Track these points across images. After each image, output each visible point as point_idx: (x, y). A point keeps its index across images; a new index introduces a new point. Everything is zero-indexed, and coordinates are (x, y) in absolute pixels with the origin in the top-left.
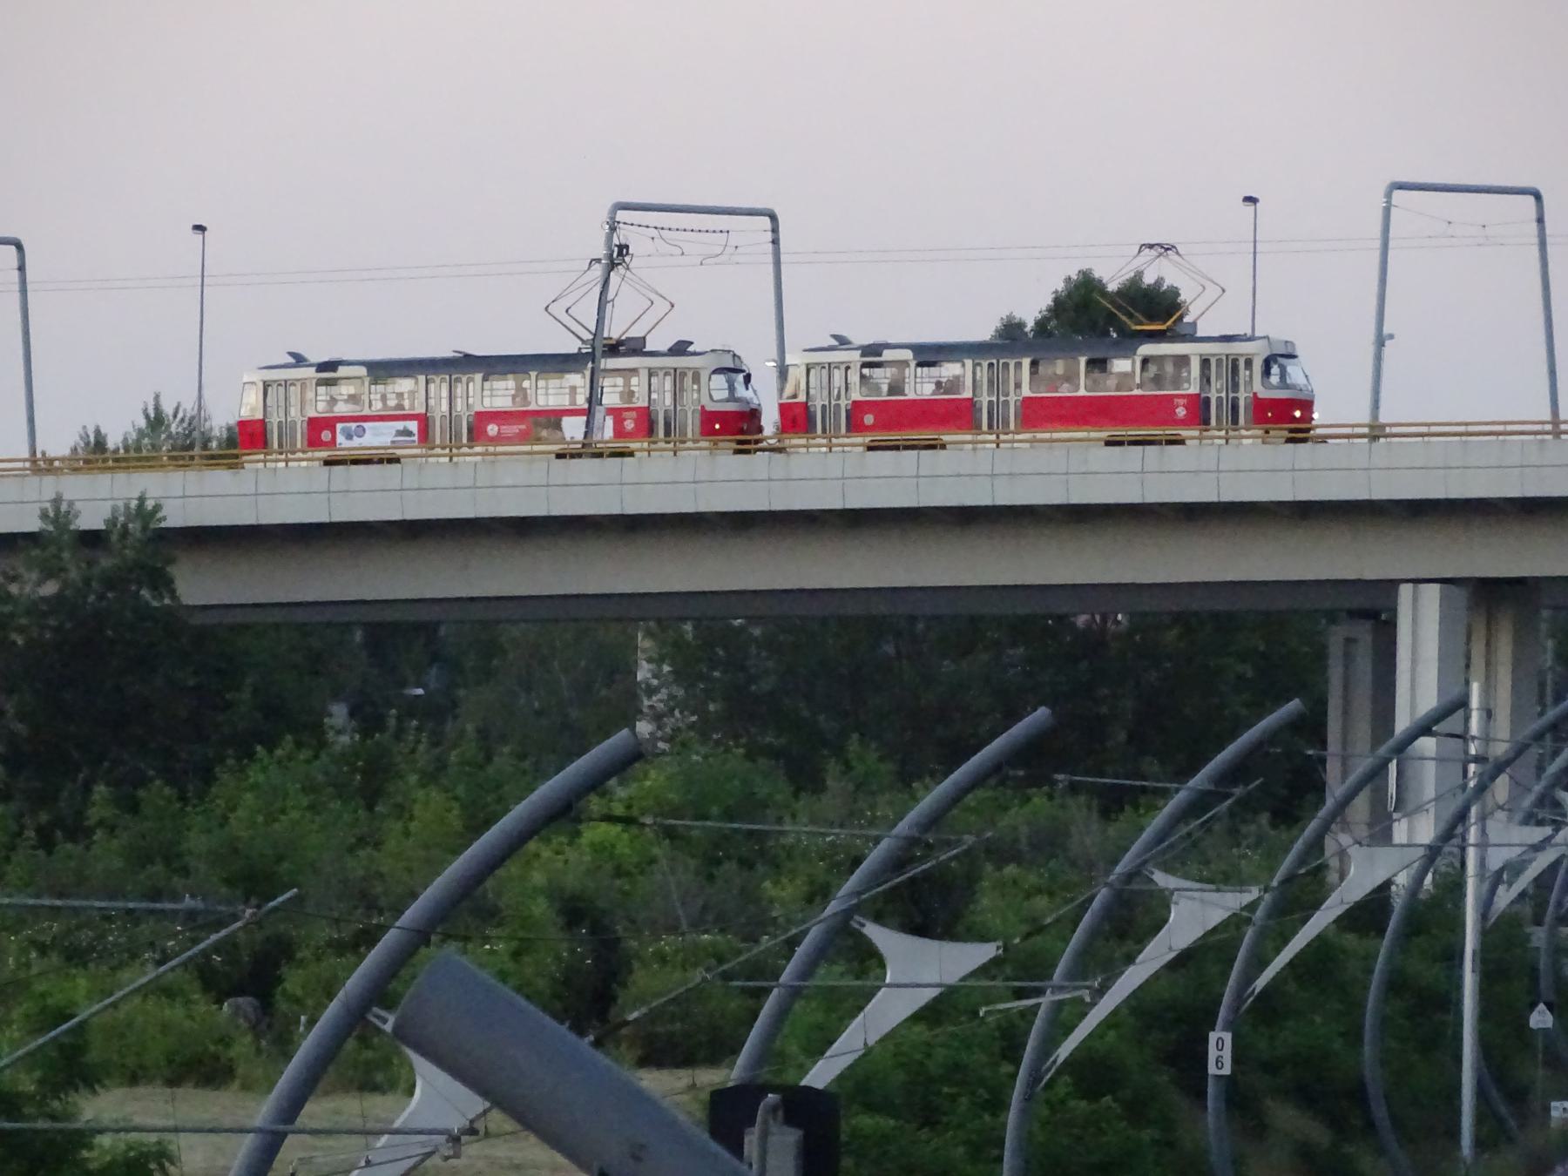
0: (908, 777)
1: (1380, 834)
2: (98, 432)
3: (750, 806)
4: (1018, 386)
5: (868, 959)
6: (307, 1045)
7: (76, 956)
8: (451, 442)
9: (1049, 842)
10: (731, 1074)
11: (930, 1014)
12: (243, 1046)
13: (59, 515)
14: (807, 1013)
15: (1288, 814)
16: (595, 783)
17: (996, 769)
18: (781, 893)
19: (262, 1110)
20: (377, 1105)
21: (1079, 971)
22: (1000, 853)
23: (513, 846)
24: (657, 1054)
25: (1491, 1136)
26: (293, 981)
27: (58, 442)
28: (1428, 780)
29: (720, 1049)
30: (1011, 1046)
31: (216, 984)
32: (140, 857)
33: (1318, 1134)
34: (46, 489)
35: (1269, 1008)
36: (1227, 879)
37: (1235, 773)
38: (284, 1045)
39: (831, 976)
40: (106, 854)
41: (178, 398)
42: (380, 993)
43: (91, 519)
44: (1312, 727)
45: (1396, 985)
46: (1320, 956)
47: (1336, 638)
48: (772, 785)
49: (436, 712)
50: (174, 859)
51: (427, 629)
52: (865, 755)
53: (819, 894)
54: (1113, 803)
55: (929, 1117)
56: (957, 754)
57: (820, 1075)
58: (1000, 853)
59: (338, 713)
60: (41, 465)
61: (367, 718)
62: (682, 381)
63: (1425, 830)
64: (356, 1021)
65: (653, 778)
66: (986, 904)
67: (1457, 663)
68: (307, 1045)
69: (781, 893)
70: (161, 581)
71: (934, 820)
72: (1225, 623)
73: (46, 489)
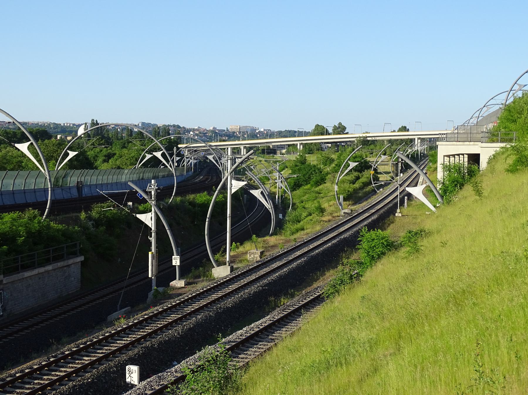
2: (340, 124)
43: (364, 136)
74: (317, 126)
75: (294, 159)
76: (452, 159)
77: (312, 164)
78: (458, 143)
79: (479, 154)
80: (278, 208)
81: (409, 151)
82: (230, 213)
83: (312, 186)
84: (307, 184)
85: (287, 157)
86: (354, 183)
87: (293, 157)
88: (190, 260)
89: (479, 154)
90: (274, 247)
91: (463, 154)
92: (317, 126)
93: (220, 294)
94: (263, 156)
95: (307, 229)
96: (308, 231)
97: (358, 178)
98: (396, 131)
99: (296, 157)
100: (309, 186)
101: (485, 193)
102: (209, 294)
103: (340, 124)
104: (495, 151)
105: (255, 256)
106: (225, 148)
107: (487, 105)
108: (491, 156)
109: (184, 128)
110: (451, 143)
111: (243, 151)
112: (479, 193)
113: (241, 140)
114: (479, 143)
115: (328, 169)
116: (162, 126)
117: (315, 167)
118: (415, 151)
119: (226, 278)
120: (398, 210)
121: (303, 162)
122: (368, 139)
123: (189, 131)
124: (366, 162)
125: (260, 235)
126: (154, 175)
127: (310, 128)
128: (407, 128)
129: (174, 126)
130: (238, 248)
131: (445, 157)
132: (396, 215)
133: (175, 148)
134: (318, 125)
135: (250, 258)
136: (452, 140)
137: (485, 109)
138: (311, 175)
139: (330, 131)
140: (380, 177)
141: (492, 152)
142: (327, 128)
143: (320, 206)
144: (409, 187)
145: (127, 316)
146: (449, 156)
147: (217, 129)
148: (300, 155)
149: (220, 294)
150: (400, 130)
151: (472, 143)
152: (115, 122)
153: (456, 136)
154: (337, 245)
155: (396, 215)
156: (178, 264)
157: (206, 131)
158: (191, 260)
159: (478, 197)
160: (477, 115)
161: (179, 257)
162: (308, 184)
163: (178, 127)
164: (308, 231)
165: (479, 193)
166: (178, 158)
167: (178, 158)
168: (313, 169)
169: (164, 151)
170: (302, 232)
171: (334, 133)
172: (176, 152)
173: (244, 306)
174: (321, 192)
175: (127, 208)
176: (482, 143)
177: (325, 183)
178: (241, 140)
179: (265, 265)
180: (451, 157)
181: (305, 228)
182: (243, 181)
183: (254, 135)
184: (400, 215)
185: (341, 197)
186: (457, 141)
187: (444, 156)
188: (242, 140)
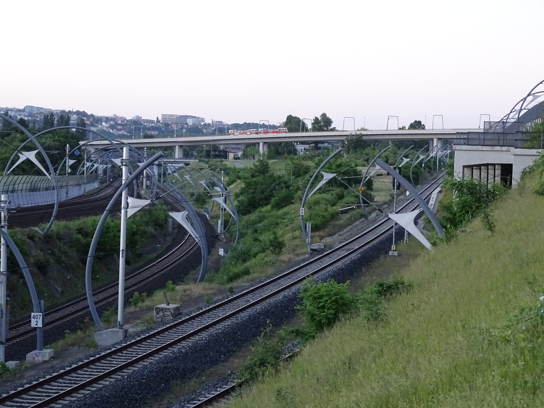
0: (405, 149)
1: (433, 153)
2: (324, 115)
3: (396, 151)
4: (57, 290)
5: (403, 160)
6: (370, 165)
7: (357, 159)
8: (424, 199)
9: (414, 153)
10: (395, 166)
11: (406, 163)
12: (366, 165)
13: (356, 134)
14: (399, 163)
15: (427, 152)
16: (387, 149)
17: (410, 149)
18: (398, 156)
19: (368, 168)
20: (374, 168)
21: (415, 160)
22: (410, 154)
23: (382, 153)
24: (390, 165)
25: (439, 170)
26: (369, 161)
27: (356, 129)
28: (435, 150)
29: (394, 165)
30: (411, 165)
31: (365, 161)
32: (360, 153)
33: (429, 170)
34: (355, 132)
35: (426, 163)
36: (424, 155)
37: (424, 149)
38: (369, 164)
39: (401, 161)
40: (359, 153)
41: (363, 127)
42: (374, 161)
43: (358, 134)
44: (429, 146)
45: (433, 161)
46: (429, 160)
47: (430, 141)
48: (397, 149)
49: (378, 145)
50: (363, 154)
51: (377, 140)
52: (403, 148)
53: (400, 156)
54: (417, 151)
55: (406, 169)
56: (408, 148)
57: (400, 166)
58: (410, 154)
59: (372, 145)
60: (355, 131)
61: (374, 145)
62: (323, 250)
63: (435, 153)
64: (373, 163)
65: (391, 149)
66: (410, 156)
67: (437, 143)
68: (370, 165)
69: (398, 156)
70: (362, 137)
71: (407, 151)
72: (424, 140)
73: (355, 132)
74: (290, 118)
75: (252, 166)
76: (476, 172)
77: (277, 175)
78: (485, 148)
79: (512, 165)
80: (219, 240)
81: (422, 157)
82: (123, 245)
83: (273, 207)
84: (267, 204)
85: (240, 164)
86: (333, 205)
87: (249, 164)
88: (68, 319)
89: (512, 165)
90: (198, 299)
91: (494, 165)
92: (290, 118)
93: (96, 373)
94: (206, 160)
95: (254, 273)
96: (255, 275)
97: (341, 197)
98: (407, 128)
99: (254, 164)
100: (269, 207)
101: (499, 227)
102: (78, 374)
103: (324, 115)
104: (535, 162)
105: (166, 313)
106: (144, 148)
107: (532, 93)
108: (525, 169)
109: (92, 116)
110: (475, 148)
111: (178, 153)
112: (491, 227)
113: (175, 136)
114: (512, 149)
115: (300, 182)
116: (60, 113)
117: (281, 178)
118: (432, 157)
119: (110, 349)
120: (393, 247)
121: (263, 169)
122: (364, 138)
123: (98, 120)
124: (356, 173)
125: (184, 280)
126: (33, 186)
127: (279, 120)
128: (422, 124)
129: (78, 113)
130: (143, 301)
131: (465, 169)
132: (391, 253)
133: (68, 145)
134: (291, 116)
135: (158, 316)
136: (477, 142)
137: (531, 98)
138: (274, 191)
139: (310, 126)
140: (375, 196)
141: (529, 162)
142: (304, 120)
143: (276, 238)
144: (402, 213)
145: (145, 367)
146: (471, 167)
147: (143, 119)
148: (259, 160)
149: (96, 373)
150: (412, 126)
151: (504, 148)
152: (61, 108)
153: (482, 137)
154: (292, 298)
155: (390, 254)
156: (40, 325)
157: (125, 122)
158: (71, 317)
159: (489, 233)
160: (518, 107)
161: (41, 314)
162: (268, 204)
163: (84, 114)
164: (255, 275)
165: (491, 227)
166: (72, 162)
167: (72, 162)
168: (277, 182)
169: (41, 149)
170: (246, 277)
171: (314, 129)
172: (69, 152)
173: (130, 395)
174: (285, 217)
175: (229, 219)
176: (515, 148)
177: (293, 203)
178: (175, 136)
179: (174, 329)
180: (474, 168)
181: (251, 271)
182: (146, 199)
183: (196, 130)
184: (396, 253)
185: (309, 225)
186: (483, 145)
187: (464, 167)
188: (177, 136)
